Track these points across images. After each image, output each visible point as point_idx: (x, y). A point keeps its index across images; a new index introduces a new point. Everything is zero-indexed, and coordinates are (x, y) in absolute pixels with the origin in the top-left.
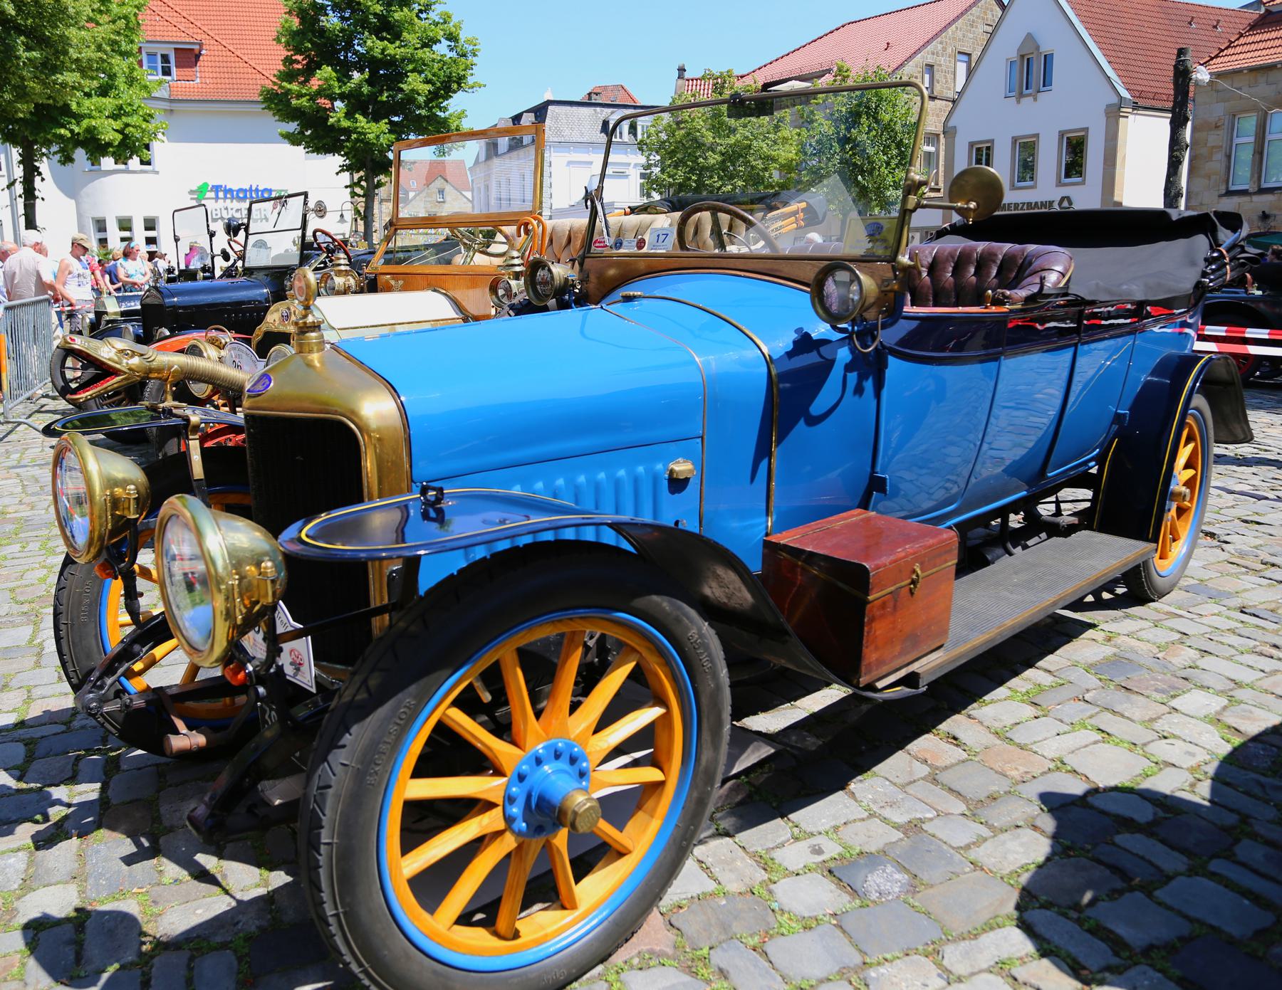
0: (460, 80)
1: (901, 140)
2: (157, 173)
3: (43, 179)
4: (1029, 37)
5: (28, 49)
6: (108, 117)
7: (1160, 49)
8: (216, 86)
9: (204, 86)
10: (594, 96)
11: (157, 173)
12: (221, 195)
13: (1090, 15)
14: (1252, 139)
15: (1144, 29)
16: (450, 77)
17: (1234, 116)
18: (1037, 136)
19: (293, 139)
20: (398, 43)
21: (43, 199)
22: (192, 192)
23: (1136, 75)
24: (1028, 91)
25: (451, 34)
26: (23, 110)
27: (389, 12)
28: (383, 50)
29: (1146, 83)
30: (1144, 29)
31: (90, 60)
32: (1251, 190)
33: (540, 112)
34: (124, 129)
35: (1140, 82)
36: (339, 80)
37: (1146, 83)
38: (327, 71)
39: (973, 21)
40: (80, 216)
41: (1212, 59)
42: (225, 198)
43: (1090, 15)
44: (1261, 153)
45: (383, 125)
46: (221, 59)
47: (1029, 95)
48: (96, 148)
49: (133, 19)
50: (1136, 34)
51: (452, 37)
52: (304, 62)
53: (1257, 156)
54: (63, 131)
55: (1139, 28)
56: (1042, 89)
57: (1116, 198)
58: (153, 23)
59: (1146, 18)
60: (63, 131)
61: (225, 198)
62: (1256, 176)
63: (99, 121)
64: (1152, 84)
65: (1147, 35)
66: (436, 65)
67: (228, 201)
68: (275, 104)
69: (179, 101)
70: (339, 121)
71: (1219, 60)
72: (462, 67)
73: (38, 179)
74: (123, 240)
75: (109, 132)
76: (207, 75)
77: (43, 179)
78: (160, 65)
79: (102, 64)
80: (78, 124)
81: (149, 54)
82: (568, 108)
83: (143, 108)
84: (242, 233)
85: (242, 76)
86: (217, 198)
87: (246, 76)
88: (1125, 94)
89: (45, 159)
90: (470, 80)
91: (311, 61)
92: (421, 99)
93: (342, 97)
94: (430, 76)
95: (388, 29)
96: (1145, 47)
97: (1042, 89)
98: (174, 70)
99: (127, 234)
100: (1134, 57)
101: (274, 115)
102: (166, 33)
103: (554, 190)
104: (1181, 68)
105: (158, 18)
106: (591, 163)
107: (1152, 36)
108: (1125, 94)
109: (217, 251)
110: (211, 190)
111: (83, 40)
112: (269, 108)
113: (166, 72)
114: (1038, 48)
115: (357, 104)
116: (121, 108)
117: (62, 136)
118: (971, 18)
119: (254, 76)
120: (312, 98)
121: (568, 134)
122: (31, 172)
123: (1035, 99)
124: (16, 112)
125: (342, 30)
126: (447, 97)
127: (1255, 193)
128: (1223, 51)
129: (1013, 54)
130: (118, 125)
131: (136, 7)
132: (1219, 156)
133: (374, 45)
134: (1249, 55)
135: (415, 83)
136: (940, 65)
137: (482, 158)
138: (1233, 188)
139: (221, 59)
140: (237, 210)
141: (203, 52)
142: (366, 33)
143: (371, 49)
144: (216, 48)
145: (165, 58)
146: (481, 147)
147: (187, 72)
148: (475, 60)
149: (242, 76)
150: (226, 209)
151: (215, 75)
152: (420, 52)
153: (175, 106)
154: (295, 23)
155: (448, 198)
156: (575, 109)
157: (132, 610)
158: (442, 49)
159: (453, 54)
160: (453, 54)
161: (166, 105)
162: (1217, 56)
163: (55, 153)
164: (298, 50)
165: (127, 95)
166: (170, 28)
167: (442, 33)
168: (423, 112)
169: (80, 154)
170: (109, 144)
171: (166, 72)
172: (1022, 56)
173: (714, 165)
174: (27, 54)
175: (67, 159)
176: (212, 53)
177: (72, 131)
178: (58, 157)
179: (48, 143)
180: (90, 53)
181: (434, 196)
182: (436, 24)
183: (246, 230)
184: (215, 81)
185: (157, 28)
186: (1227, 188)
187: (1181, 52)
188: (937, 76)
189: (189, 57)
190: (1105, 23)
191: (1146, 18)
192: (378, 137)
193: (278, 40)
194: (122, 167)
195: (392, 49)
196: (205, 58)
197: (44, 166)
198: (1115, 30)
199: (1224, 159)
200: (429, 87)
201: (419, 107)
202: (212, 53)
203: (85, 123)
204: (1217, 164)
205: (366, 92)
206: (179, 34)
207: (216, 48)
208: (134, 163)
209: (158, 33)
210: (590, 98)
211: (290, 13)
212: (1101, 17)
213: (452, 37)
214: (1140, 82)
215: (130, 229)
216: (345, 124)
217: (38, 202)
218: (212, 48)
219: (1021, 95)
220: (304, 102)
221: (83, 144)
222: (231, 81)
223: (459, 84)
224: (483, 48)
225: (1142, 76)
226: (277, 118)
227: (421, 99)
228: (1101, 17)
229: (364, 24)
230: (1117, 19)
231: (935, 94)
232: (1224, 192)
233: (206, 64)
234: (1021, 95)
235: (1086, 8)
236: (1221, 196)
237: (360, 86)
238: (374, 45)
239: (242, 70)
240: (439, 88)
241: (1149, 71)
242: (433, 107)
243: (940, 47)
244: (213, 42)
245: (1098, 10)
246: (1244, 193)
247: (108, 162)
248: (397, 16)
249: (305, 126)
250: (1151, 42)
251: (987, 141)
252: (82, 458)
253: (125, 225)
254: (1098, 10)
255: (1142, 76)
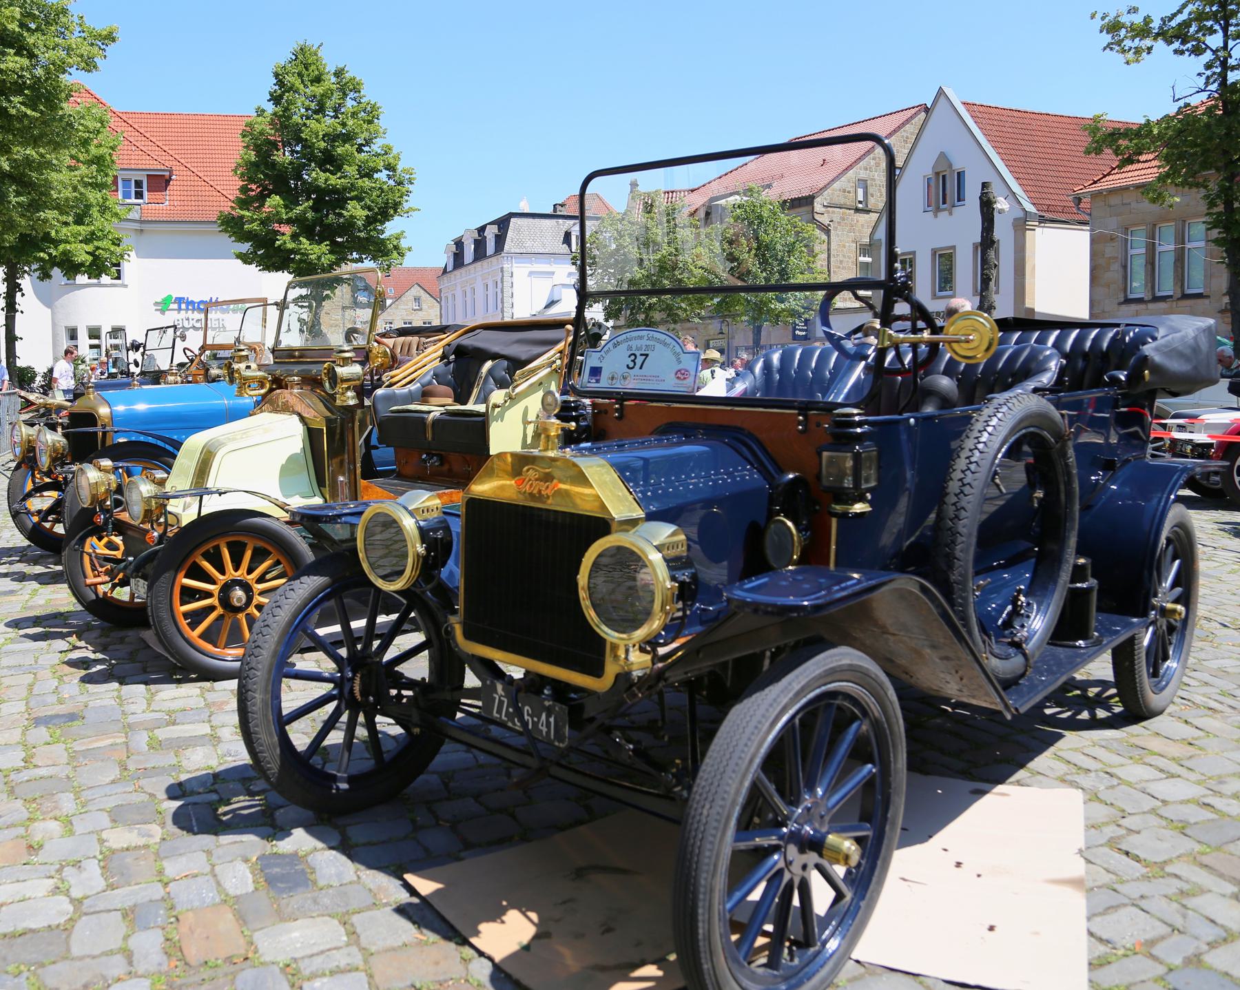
0: (396, 206)
1: (782, 257)
2: (126, 286)
3: (23, 295)
4: (943, 156)
5: (18, 194)
6: (81, 242)
7: (1074, 165)
8: (183, 208)
9: (172, 208)
10: (559, 208)
11: (126, 286)
12: (183, 306)
13: (1001, 134)
14: (1143, 251)
15: (1057, 146)
16: (387, 203)
17: (1155, 225)
18: (954, 247)
19: (245, 259)
20: (339, 175)
21: (22, 312)
22: (156, 304)
23: (1046, 190)
24: (945, 206)
25: (389, 164)
26: (10, 239)
27: (333, 146)
28: (326, 180)
29: (1055, 197)
30: (1057, 146)
31: (67, 199)
32: (1146, 298)
33: (503, 224)
34: (95, 251)
35: (1049, 196)
36: (286, 207)
37: (1055, 197)
38: (275, 200)
39: (907, 138)
40: (54, 325)
41: (1105, 176)
42: (187, 309)
43: (1001, 134)
44: (1153, 264)
45: (324, 247)
46: (189, 183)
47: (944, 210)
48: (71, 268)
49: (108, 158)
50: (1049, 151)
51: (390, 167)
52: (259, 190)
53: (1149, 267)
54: (42, 254)
55: (1051, 145)
56: (957, 203)
57: (1028, 305)
58: (130, 153)
59: (1061, 136)
60: (42, 254)
61: (187, 309)
62: (1150, 285)
63: (73, 246)
64: (1062, 198)
65: (1061, 152)
66: (374, 194)
67: (190, 312)
68: (231, 227)
69: (149, 222)
70: (285, 243)
71: (1111, 177)
72: (398, 195)
73: (18, 294)
74: (92, 347)
75: (81, 254)
76: (175, 198)
77: (23, 295)
78: (133, 190)
79: (82, 198)
80: (56, 247)
81: (124, 180)
82: (531, 220)
83: (112, 233)
84: (141, 350)
85: (207, 198)
86: (180, 309)
87: (211, 199)
88: (1031, 208)
89: (26, 275)
90: (406, 206)
91: (265, 189)
92: (360, 223)
93: (289, 221)
94: (369, 203)
95: (330, 161)
96: (1056, 163)
97: (957, 203)
98: (146, 194)
99: (96, 342)
100: (1045, 173)
101: (230, 237)
102: (140, 162)
103: (515, 300)
104: (985, 199)
105: (134, 148)
106: (553, 273)
107: (1066, 152)
108: (1031, 208)
109: (131, 360)
110: (175, 302)
111: (61, 182)
112: (225, 231)
113: (139, 195)
114: (950, 166)
115: (306, 229)
116: (93, 233)
117: (42, 259)
118: (905, 134)
119: (218, 199)
120: (263, 223)
121: (530, 246)
122: (13, 289)
123: (951, 214)
124: (3, 241)
125: (291, 163)
126: (382, 223)
127: (1149, 301)
128: (1114, 169)
129: (929, 172)
130: (89, 248)
131: (112, 148)
132: (1116, 267)
133: (317, 176)
134: (1136, 173)
135: (356, 211)
136: (874, 180)
137: (450, 268)
138: (1159, 294)
139: (189, 183)
140: (198, 321)
141: (173, 177)
142: (313, 165)
143: (316, 179)
144: (185, 173)
145: (138, 184)
146: (448, 257)
147: (158, 195)
148: (410, 187)
149: (207, 198)
150: (188, 319)
151: (182, 198)
152: (360, 181)
153: (145, 227)
154: (252, 156)
155: (424, 306)
156: (537, 221)
157: (34, 482)
158: (382, 176)
159: (391, 182)
160: (391, 182)
161: (137, 226)
162: (1109, 174)
163: (36, 270)
164: (251, 180)
165: (98, 221)
166: (144, 157)
167: (382, 164)
168: (362, 235)
169: (56, 272)
170: (82, 264)
171: (139, 195)
172: (937, 174)
173: (640, 279)
174: (17, 199)
175: (45, 276)
176: (181, 178)
177: (50, 255)
178: (37, 274)
179: (29, 264)
180: (68, 193)
181: (410, 304)
182: (377, 155)
183: (144, 347)
184: (182, 203)
185: (133, 157)
186: (1126, 296)
187: (985, 185)
188: (870, 190)
189: (160, 182)
190: (1016, 141)
191: (1061, 136)
192: (319, 258)
193: (235, 171)
194: (95, 281)
195: (334, 180)
196: (175, 183)
197: (26, 282)
198: (1026, 148)
199: (1121, 269)
200: (366, 212)
201: (360, 231)
202: (181, 178)
203: (61, 247)
204: (1114, 273)
205: (310, 217)
206: (151, 162)
207: (185, 173)
208: (105, 279)
209: (133, 162)
210: (555, 210)
211: (247, 147)
212: (1012, 135)
213: (390, 167)
214: (1049, 196)
215: (98, 337)
216: (290, 245)
217: (18, 315)
218: (181, 173)
219: (938, 210)
220: (255, 226)
221: (59, 265)
222: (197, 203)
223: (396, 211)
224: (418, 177)
225: (1052, 191)
226: (233, 238)
227: (360, 223)
228: (1012, 135)
229: (311, 158)
230: (1030, 138)
231: (870, 207)
232: (1122, 300)
233: (175, 188)
234: (938, 210)
235: (997, 128)
236: (1120, 304)
237: (304, 212)
238: (317, 176)
239: (207, 193)
240: (376, 214)
241: (1060, 186)
242: (371, 230)
243: (873, 162)
244: (182, 168)
245: (1009, 130)
246: (1140, 301)
247: (82, 279)
248: (339, 150)
249: (257, 246)
250: (1064, 158)
251: (909, 253)
252: (20, 427)
253: (94, 333)
254: (1009, 130)
255: (1052, 191)
